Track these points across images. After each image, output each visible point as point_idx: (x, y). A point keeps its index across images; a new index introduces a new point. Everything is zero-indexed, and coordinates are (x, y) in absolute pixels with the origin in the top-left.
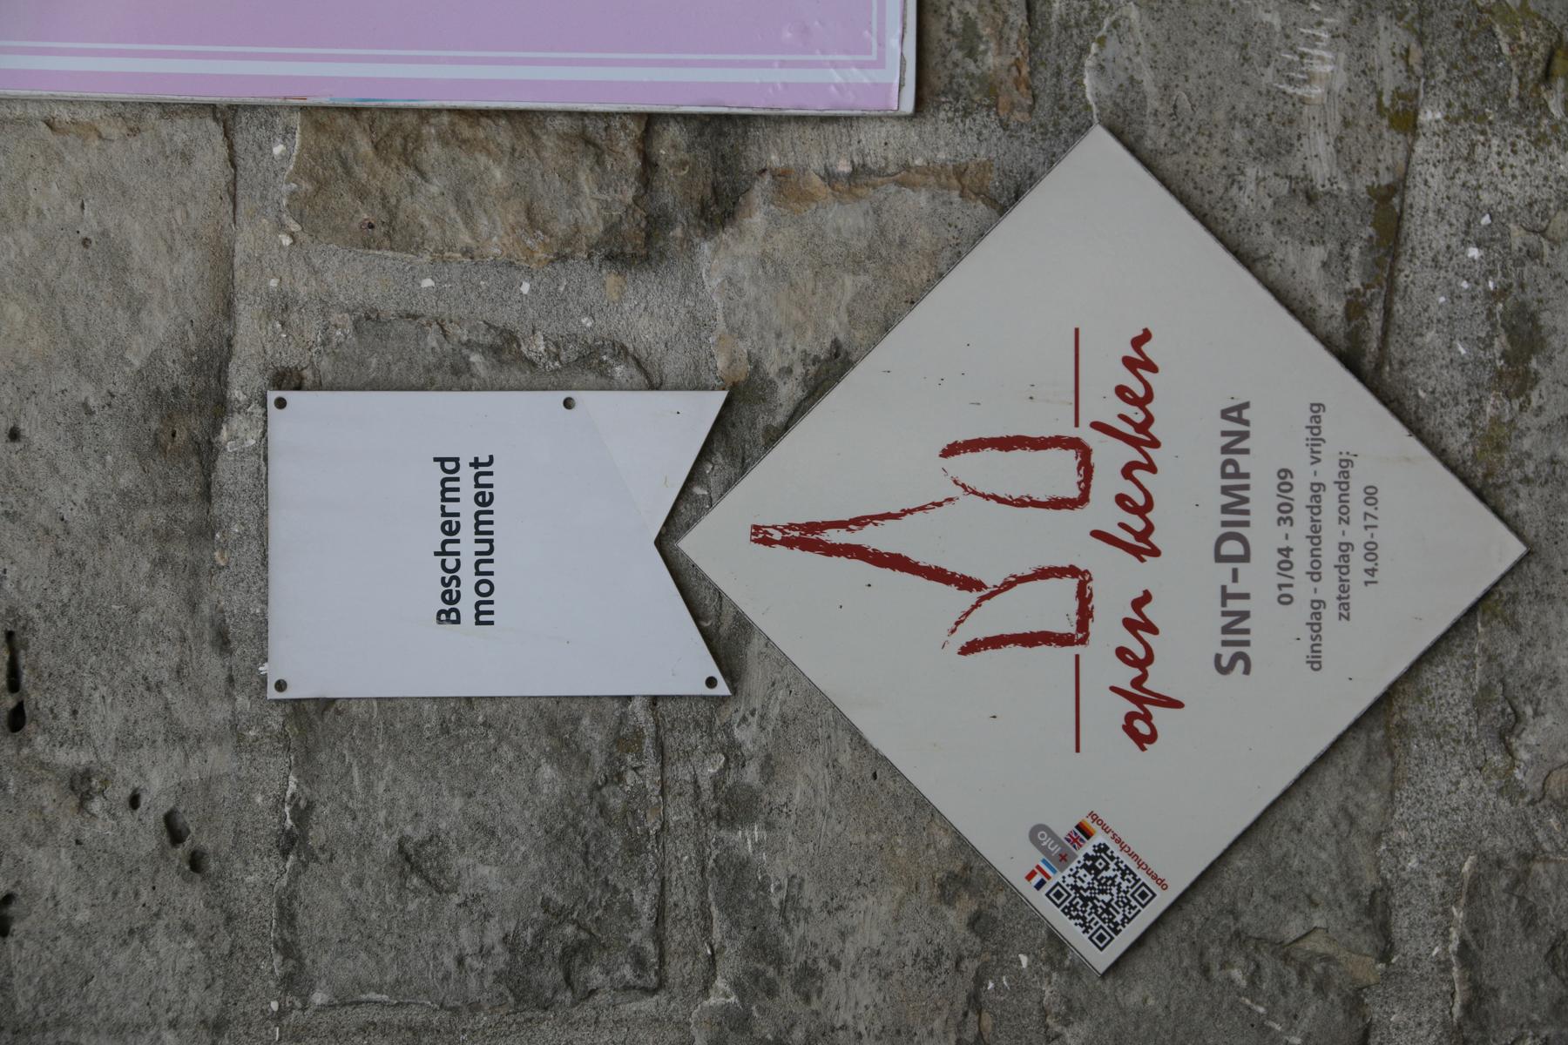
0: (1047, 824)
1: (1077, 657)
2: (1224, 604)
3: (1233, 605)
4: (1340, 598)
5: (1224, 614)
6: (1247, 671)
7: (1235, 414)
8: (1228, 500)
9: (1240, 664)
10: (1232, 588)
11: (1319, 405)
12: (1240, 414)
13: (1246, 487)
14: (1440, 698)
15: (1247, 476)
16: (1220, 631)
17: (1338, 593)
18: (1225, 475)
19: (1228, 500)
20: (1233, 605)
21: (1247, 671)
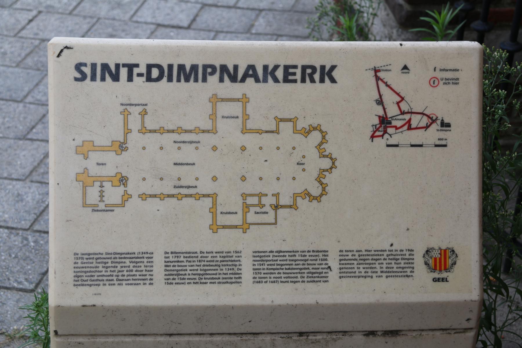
0: (434, 278)
1: (237, 117)
2: (124, 65)
3: (123, 72)
4: (258, 256)
5: (117, 66)
6: (76, 79)
7: (251, 72)
8: (188, 68)
9: (78, 76)
10: (136, 71)
11: (372, 277)
12: (251, 76)
13: (196, 80)
14: (393, 224)
15: (204, 80)
16: (105, 62)
17: (99, 271)
18: (205, 67)
19: (188, 68)
20: (123, 72)
21: (76, 79)
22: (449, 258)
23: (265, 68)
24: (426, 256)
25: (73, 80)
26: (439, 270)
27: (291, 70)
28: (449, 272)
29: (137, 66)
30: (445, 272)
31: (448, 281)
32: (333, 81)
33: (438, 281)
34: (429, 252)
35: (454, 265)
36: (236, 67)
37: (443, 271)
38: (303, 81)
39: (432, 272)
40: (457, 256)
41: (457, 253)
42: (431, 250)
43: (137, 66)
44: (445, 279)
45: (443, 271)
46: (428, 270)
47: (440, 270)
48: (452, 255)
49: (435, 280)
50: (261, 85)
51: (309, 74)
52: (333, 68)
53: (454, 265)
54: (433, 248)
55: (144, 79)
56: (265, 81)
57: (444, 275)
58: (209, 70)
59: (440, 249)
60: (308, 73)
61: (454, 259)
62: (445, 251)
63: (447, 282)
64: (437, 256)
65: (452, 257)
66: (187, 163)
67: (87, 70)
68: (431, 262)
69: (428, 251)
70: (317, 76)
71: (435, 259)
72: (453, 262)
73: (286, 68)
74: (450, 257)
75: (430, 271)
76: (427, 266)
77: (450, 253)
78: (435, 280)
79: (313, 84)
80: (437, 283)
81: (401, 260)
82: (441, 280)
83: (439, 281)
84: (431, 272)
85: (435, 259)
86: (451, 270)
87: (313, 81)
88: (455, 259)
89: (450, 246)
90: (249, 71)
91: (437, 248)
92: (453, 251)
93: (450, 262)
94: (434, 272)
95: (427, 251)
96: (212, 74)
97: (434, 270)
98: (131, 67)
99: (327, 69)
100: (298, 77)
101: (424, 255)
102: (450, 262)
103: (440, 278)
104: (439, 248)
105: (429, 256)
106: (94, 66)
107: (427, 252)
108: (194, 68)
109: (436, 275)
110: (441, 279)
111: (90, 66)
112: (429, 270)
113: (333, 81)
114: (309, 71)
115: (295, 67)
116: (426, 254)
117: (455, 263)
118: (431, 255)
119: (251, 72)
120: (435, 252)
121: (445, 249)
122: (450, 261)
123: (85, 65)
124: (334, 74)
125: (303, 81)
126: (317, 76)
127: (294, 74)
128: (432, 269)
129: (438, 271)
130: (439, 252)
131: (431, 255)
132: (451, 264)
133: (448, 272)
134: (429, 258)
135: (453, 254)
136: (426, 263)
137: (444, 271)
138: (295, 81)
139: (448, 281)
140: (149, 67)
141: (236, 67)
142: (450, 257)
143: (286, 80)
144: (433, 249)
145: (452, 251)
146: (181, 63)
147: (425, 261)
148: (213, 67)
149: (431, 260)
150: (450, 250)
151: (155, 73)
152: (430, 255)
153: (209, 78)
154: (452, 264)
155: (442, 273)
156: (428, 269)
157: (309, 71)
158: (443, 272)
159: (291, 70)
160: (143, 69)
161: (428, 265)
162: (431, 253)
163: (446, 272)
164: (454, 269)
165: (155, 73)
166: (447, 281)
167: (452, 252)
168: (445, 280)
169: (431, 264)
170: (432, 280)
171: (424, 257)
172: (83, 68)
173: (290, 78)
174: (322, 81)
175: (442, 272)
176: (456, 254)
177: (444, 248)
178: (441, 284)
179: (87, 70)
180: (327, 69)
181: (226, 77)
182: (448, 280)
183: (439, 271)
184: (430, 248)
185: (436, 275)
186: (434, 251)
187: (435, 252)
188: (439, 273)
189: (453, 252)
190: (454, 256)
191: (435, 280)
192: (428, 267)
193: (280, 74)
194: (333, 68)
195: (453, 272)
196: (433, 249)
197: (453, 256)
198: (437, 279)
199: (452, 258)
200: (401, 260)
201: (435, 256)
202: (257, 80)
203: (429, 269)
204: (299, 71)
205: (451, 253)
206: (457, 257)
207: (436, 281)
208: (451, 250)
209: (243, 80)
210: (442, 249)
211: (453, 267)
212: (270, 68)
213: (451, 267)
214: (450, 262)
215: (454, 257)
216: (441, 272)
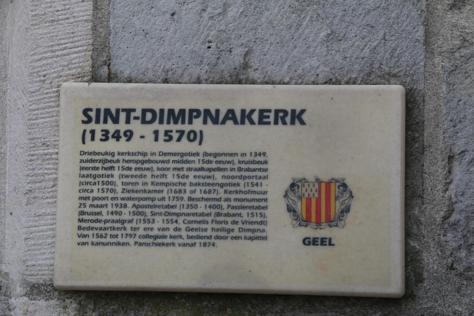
2: (124, 110)
7: (230, 116)
8: (177, 112)
9: (85, 119)
10: (133, 115)
12: (230, 119)
18: (191, 111)
19: (177, 112)
22: (336, 199)
23: (243, 111)
24: (291, 195)
25: (81, 122)
26: (316, 223)
27: (266, 114)
28: (336, 226)
29: (134, 110)
30: (328, 227)
31: (334, 245)
32: (302, 123)
33: (314, 244)
34: (296, 188)
35: (345, 214)
36: (218, 111)
37: (324, 225)
38: (276, 123)
39: (301, 226)
40: (351, 196)
41: (351, 189)
42: (300, 184)
43: (134, 110)
44: (328, 241)
45: (324, 225)
46: (294, 222)
47: (318, 223)
48: (342, 194)
49: (308, 241)
50: (240, 127)
51: (281, 117)
52: (303, 111)
53: (345, 214)
54: (305, 179)
55: (139, 121)
56: (243, 123)
57: (324, 232)
58: (195, 114)
59: (318, 181)
60: (280, 117)
61: (347, 202)
62: (328, 184)
63: (331, 247)
64: (311, 196)
65: (341, 197)
66: (94, 152)
67: (93, 114)
68: (300, 207)
69: (295, 186)
70: (288, 119)
71: (309, 200)
72: (343, 207)
73: (262, 112)
74: (338, 196)
75: (298, 223)
76: (292, 213)
77: (337, 190)
78: (307, 242)
79: (285, 126)
80: (312, 247)
81: (159, 155)
82: (319, 243)
83: (316, 243)
84: (300, 225)
85: (309, 200)
86: (339, 224)
87: (284, 123)
88: (348, 200)
89: (337, 176)
90: (229, 115)
91: (311, 178)
92: (344, 186)
93: (338, 208)
94: (306, 226)
95: (293, 185)
96: (197, 117)
97: (306, 222)
98: (129, 111)
99: (297, 112)
100: (272, 119)
101: (286, 192)
102: (338, 208)
103: (318, 238)
104: (316, 180)
105: (295, 194)
106: (98, 111)
107: (293, 187)
108: (182, 112)
109: (310, 232)
110: (319, 240)
111: (95, 111)
112: (296, 221)
113: (302, 123)
114: (281, 114)
115: (269, 111)
116: (290, 191)
117: (347, 210)
118: (300, 192)
119: (230, 116)
120: (309, 186)
121: (328, 181)
122: (338, 204)
123: (91, 110)
124: (304, 117)
125: (276, 123)
126: (288, 119)
127: (268, 117)
128: (302, 221)
129: (313, 225)
130: (317, 186)
131: (300, 192)
132: (340, 211)
133: (334, 227)
134: (296, 199)
135: (344, 191)
136: (290, 209)
137: (325, 224)
138: (269, 123)
139: (334, 245)
140: (144, 111)
141: (218, 111)
142: (338, 196)
143: (261, 122)
144: (304, 181)
145: (342, 186)
146: (171, 107)
147: (287, 204)
148: (198, 111)
149: (299, 204)
150: (338, 184)
151: (149, 116)
152: (298, 193)
153: (195, 120)
154: (342, 212)
155: (320, 229)
156: (294, 220)
157: (281, 114)
158: (323, 227)
159: (266, 114)
160: (138, 113)
161: (295, 211)
162: (300, 189)
163: (331, 226)
164: (346, 220)
165: (149, 116)
166: (330, 244)
167: (341, 188)
168: (327, 243)
169: (300, 211)
170: (302, 241)
171: (286, 196)
172: (90, 113)
173: (265, 120)
174: (293, 123)
175: (321, 227)
176: (351, 192)
177: (325, 178)
178: (319, 250)
179: (93, 114)
180: (297, 112)
181: (209, 121)
182: (333, 242)
183: (315, 224)
184: (298, 180)
185: (310, 232)
186: (306, 185)
187: (309, 186)
188: (317, 227)
189: (344, 187)
190: (346, 195)
191: (306, 242)
192: (293, 215)
193: (255, 117)
194: (303, 111)
195: (343, 227)
196: (304, 180)
197: (345, 195)
198: (311, 240)
199: (341, 200)
200: (159, 155)
201: (309, 196)
202: (236, 122)
203: (296, 220)
204: (272, 115)
205: (339, 189)
206: (353, 197)
207: (309, 244)
208: (340, 184)
209: (223, 122)
210: (321, 182)
211: (343, 216)
212: (247, 112)
213: (339, 217)
214: (336, 207)
215: (345, 198)
216: (320, 225)
